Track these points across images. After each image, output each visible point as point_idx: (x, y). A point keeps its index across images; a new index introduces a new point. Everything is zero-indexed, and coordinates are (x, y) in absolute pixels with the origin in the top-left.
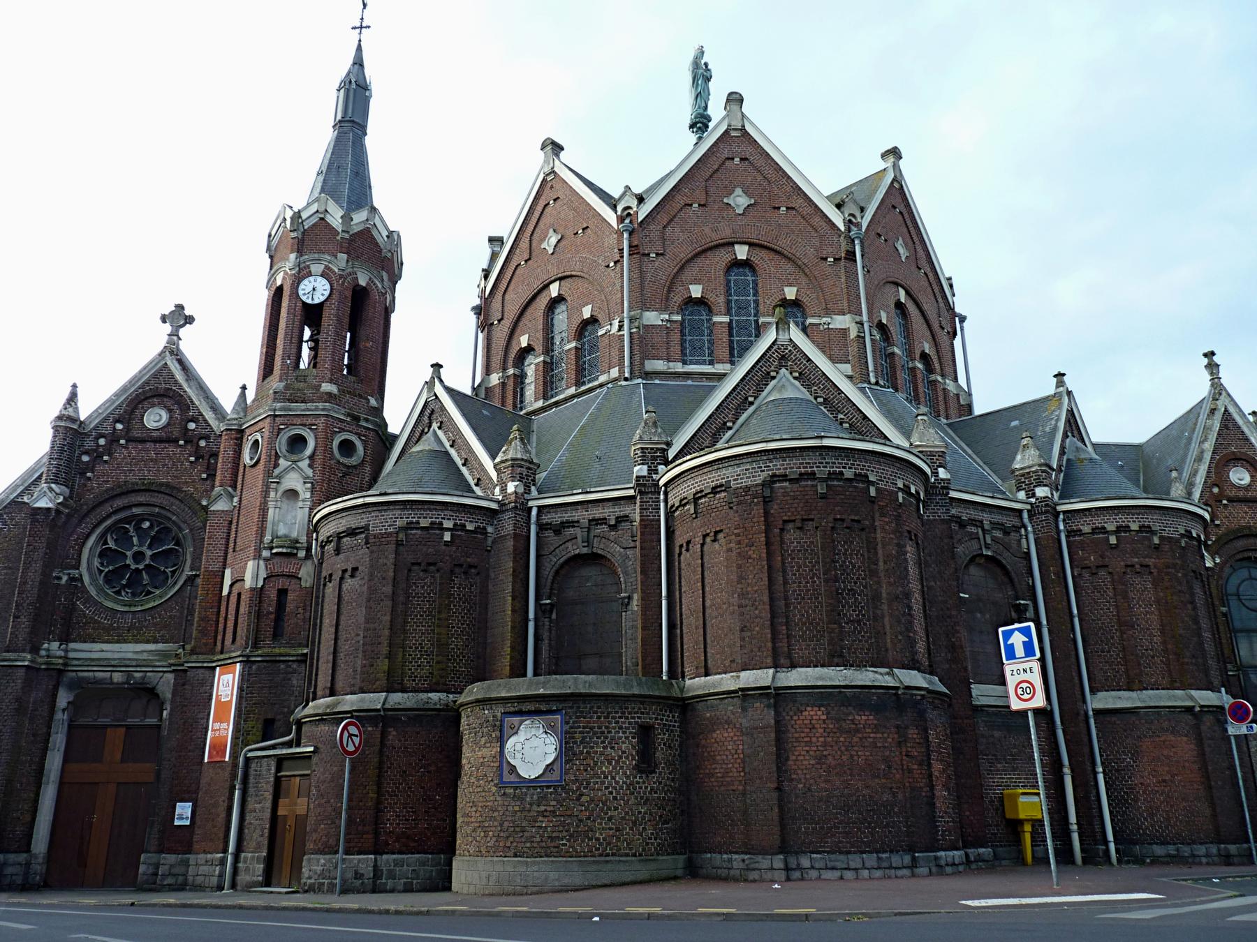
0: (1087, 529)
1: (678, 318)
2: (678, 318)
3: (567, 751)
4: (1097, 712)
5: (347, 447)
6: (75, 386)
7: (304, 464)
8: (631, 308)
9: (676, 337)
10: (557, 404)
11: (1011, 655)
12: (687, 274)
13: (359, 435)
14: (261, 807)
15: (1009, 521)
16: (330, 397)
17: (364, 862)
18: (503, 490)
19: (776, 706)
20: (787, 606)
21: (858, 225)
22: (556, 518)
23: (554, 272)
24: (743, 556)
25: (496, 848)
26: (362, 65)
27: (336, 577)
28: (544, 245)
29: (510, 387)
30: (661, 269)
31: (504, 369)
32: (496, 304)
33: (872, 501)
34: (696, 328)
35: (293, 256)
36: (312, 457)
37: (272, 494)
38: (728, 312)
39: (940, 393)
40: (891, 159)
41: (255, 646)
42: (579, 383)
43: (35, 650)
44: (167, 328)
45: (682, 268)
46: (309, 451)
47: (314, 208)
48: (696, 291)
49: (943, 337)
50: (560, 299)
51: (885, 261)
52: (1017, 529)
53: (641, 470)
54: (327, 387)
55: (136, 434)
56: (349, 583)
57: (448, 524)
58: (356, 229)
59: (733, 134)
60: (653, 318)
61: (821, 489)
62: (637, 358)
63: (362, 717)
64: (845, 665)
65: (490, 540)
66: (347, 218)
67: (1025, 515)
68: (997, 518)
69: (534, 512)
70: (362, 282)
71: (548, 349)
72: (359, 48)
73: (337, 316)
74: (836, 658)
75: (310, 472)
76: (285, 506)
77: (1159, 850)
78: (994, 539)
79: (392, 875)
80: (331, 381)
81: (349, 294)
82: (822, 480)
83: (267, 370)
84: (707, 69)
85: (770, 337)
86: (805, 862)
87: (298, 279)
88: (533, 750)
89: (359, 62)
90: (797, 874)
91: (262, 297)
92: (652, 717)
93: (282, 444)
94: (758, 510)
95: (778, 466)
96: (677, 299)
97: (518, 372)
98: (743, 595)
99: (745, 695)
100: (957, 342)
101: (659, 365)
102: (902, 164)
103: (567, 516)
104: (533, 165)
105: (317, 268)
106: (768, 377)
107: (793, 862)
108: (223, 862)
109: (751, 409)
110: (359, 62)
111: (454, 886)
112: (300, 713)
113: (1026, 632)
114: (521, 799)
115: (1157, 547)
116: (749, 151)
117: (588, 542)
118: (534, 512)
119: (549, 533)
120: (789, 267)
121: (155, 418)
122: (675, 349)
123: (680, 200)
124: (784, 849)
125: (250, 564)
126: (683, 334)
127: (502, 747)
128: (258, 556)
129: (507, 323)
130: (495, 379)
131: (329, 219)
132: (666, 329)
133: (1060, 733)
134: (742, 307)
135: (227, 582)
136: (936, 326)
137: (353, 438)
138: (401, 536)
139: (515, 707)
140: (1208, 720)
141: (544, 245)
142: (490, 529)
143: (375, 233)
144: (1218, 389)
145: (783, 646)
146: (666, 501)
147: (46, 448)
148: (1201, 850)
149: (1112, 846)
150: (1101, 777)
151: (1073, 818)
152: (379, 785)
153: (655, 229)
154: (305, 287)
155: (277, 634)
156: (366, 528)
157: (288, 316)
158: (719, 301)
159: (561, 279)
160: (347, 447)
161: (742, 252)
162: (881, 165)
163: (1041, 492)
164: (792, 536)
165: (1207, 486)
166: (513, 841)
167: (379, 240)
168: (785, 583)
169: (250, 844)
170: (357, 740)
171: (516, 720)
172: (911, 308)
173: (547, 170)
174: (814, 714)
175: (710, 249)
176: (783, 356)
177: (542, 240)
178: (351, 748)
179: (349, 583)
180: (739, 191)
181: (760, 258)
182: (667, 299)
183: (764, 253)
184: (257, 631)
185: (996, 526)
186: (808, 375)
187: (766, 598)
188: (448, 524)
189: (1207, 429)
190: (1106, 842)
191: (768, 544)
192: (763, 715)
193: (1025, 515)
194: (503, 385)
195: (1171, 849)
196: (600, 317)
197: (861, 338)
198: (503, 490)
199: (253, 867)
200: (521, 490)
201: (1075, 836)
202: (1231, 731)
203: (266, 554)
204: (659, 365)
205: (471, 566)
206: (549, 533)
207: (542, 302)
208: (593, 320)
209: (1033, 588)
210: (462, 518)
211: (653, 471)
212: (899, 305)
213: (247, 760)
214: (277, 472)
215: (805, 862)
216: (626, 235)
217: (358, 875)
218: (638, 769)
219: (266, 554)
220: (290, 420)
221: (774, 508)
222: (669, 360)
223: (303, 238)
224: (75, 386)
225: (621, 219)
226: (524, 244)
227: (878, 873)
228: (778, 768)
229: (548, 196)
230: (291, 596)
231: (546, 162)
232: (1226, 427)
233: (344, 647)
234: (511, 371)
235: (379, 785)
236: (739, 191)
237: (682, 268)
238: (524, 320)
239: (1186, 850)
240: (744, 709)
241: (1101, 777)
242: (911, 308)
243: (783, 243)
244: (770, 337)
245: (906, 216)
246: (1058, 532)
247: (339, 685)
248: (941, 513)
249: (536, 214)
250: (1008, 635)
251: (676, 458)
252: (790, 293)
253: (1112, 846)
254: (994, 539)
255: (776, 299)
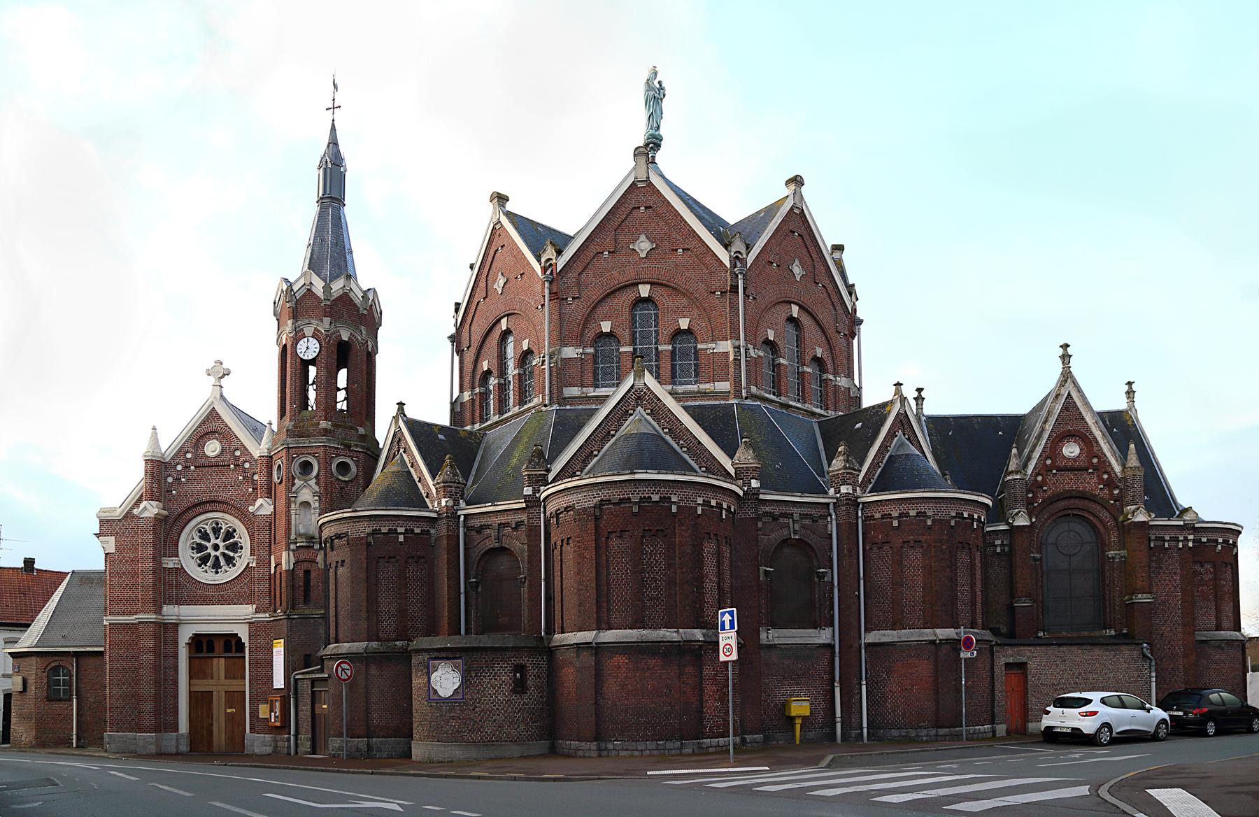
0: (878, 516)
1: (591, 350)
2: (591, 350)
3: (465, 682)
4: (868, 645)
5: (343, 467)
6: (154, 429)
7: (313, 482)
8: (550, 347)
9: (589, 366)
10: (506, 420)
11: (723, 629)
12: (599, 313)
13: (352, 457)
14: (306, 708)
15: (815, 512)
16: (326, 432)
17: (361, 742)
18: (439, 503)
19: (596, 654)
20: (609, 589)
21: (743, 261)
22: (477, 523)
23: (503, 309)
24: (581, 556)
25: (428, 736)
26: (336, 144)
27: (333, 566)
28: (495, 286)
29: (477, 403)
30: (577, 309)
31: (473, 388)
32: (465, 335)
33: (674, 515)
34: (607, 357)
35: (290, 322)
36: (317, 477)
37: (293, 506)
38: (633, 343)
39: (831, 389)
40: (793, 187)
41: (293, 608)
42: (501, 412)
43: (158, 611)
44: (212, 380)
45: (594, 308)
46: (315, 473)
47: (302, 282)
48: (606, 327)
49: (840, 340)
50: (508, 332)
51: (792, 277)
52: (825, 517)
53: (528, 491)
54: (323, 424)
55: (203, 462)
56: (341, 570)
57: (401, 530)
58: (335, 296)
59: (640, 185)
60: (570, 352)
61: (635, 509)
62: (555, 387)
63: (351, 657)
64: (644, 628)
65: (433, 540)
66: (327, 288)
67: (831, 507)
68: (806, 511)
69: (462, 518)
70: (345, 338)
71: (502, 373)
72: (333, 128)
73: (327, 368)
74: (638, 624)
75: (317, 488)
76: (302, 513)
77: (895, 733)
78: (803, 527)
79: (379, 750)
80: (326, 419)
81: (334, 349)
82: (635, 503)
83: (282, 413)
84: (661, 88)
85: (628, 383)
86: (610, 746)
87: (296, 340)
88: (446, 680)
89: (333, 142)
90: (605, 753)
91: (276, 351)
92: (527, 661)
93: (296, 469)
94: (591, 525)
95: (605, 494)
96: (590, 334)
97: (483, 390)
98: (580, 583)
99: (578, 647)
100: (855, 341)
101: (574, 391)
102: (804, 190)
103: (483, 521)
104: (485, 215)
105: (309, 331)
106: (626, 415)
107: (603, 745)
108: (289, 740)
109: (613, 440)
110: (333, 142)
111: (414, 758)
112: (322, 653)
113: (731, 613)
114: (440, 709)
115: (930, 528)
116: (652, 200)
117: (498, 538)
118: (462, 518)
119: (473, 533)
120: (685, 302)
121: (212, 448)
122: (589, 376)
123: (593, 249)
124: (598, 737)
125: (284, 554)
126: (595, 362)
127: (429, 679)
128: (288, 549)
129: (473, 350)
130: (467, 396)
131: (314, 290)
132: (581, 360)
133: (837, 660)
134: (645, 337)
135: (273, 565)
136: (831, 331)
137: (348, 460)
138: (370, 539)
139: (435, 654)
140: (945, 649)
141: (495, 286)
142: (432, 531)
143: (351, 295)
144: (1067, 376)
145: (605, 616)
146: (545, 512)
147: (142, 475)
148: (924, 732)
149: (865, 731)
150: (864, 687)
151: (838, 714)
152: (367, 698)
153: (572, 276)
154: (302, 346)
155: (307, 600)
156: (346, 534)
157: (293, 372)
158: (625, 334)
159: (508, 315)
160: (343, 467)
161: (644, 291)
162: (785, 191)
163: (844, 489)
164: (615, 543)
165: (1043, 458)
166: (436, 735)
167: (357, 302)
168: (608, 574)
169: (302, 730)
170: (349, 673)
171: (436, 662)
172: (806, 321)
173: (495, 220)
174: (621, 660)
175: (618, 289)
176: (639, 397)
177: (495, 281)
178: (345, 677)
179: (341, 570)
180: (643, 237)
181: (662, 296)
182: (582, 335)
183: (663, 291)
184: (293, 599)
185: (803, 516)
186: (658, 410)
187: (594, 585)
188: (401, 530)
189: (1049, 413)
190: (862, 728)
191: (597, 548)
192: (588, 659)
193: (831, 507)
194: (473, 400)
195: (903, 732)
196: (535, 349)
197: (737, 361)
198: (439, 503)
199: (305, 746)
200: (451, 503)
201: (839, 726)
202: (962, 655)
203: (293, 547)
204: (574, 391)
205: (420, 557)
206: (473, 533)
207: (496, 334)
208: (529, 352)
209: (831, 559)
210: (410, 525)
211: (536, 491)
212: (791, 319)
213: (296, 680)
214: (294, 489)
215: (610, 746)
216: (547, 284)
217: (358, 750)
218: (514, 691)
219: (293, 547)
220: (300, 450)
221: (602, 523)
222: (582, 386)
223: (297, 306)
224: (154, 429)
225: (544, 270)
226: (482, 284)
227: (655, 752)
228: (596, 691)
229: (497, 243)
230: (313, 575)
231: (494, 213)
232: (1067, 409)
233: (342, 613)
234: (477, 390)
235: (367, 698)
236: (643, 237)
237: (594, 308)
238: (485, 349)
239: (913, 733)
240: (578, 656)
241: (864, 687)
242: (806, 321)
243: (679, 282)
244: (628, 383)
245: (806, 237)
246: (857, 517)
247: (341, 636)
248: (751, 514)
249: (488, 263)
250: (723, 614)
251: (553, 481)
252: (684, 324)
253: (865, 731)
254: (803, 527)
255: (672, 329)
